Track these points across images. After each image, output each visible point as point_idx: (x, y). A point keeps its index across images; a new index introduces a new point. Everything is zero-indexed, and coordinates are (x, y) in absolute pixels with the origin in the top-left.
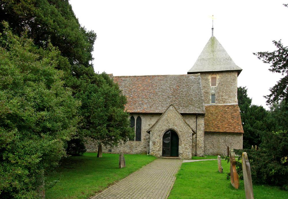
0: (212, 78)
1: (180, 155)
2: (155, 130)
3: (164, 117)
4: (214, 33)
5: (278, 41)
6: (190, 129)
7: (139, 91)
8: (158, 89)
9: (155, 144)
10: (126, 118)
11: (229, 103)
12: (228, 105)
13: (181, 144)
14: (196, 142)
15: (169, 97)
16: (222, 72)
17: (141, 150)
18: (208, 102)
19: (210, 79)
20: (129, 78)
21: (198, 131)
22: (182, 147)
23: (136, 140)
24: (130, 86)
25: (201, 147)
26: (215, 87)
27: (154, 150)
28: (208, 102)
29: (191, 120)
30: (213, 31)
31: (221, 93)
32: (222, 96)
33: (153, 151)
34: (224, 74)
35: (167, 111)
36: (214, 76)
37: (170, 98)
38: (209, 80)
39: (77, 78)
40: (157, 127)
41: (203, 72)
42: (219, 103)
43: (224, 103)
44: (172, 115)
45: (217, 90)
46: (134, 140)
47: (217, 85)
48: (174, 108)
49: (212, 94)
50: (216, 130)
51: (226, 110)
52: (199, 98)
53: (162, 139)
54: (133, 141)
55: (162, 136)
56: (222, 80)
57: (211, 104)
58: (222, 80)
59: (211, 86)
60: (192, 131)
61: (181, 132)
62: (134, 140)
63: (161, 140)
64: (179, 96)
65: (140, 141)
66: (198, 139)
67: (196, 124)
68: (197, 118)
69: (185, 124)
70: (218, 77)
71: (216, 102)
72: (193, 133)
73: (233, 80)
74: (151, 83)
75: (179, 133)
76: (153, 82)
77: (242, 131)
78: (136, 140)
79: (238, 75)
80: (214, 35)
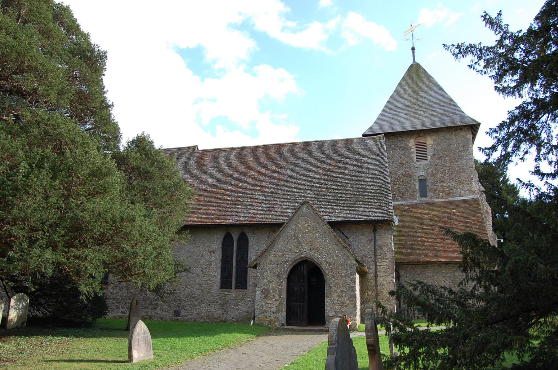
0: (417, 145)
2: (268, 261)
3: (289, 232)
4: (415, 53)
5: (493, 15)
6: (351, 258)
7: (247, 178)
8: (289, 170)
9: (267, 295)
11: (460, 196)
14: (377, 286)
15: (311, 187)
16: (437, 132)
17: (247, 311)
18: (413, 197)
19: (412, 147)
21: (380, 260)
22: (331, 300)
23: (236, 288)
24: (229, 169)
26: (425, 162)
28: (413, 197)
30: (413, 53)
31: (439, 175)
32: (443, 182)
33: (263, 313)
34: (442, 135)
35: (295, 217)
36: (421, 140)
37: (315, 189)
38: (411, 148)
40: (271, 257)
41: (397, 132)
42: (438, 196)
43: (448, 197)
44: (306, 225)
45: (430, 170)
46: (231, 288)
47: (429, 158)
48: (310, 208)
49: (420, 178)
50: (431, 258)
51: (454, 211)
52: (381, 187)
53: (284, 283)
54: (229, 290)
55: (285, 276)
56: (439, 148)
57: (419, 199)
58: (439, 148)
59: (415, 160)
60: (355, 263)
61: (329, 264)
62: (231, 288)
64: (334, 183)
65: (246, 288)
66: (381, 279)
67: (375, 245)
68: (375, 231)
69: (337, 245)
70: (430, 141)
71: (430, 194)
72: (357, 265)
73: (463, 146)
74: (276, 159)
75: (325, 268)
76: (279, 158)
78: (236, 288)
80: (417, 60)
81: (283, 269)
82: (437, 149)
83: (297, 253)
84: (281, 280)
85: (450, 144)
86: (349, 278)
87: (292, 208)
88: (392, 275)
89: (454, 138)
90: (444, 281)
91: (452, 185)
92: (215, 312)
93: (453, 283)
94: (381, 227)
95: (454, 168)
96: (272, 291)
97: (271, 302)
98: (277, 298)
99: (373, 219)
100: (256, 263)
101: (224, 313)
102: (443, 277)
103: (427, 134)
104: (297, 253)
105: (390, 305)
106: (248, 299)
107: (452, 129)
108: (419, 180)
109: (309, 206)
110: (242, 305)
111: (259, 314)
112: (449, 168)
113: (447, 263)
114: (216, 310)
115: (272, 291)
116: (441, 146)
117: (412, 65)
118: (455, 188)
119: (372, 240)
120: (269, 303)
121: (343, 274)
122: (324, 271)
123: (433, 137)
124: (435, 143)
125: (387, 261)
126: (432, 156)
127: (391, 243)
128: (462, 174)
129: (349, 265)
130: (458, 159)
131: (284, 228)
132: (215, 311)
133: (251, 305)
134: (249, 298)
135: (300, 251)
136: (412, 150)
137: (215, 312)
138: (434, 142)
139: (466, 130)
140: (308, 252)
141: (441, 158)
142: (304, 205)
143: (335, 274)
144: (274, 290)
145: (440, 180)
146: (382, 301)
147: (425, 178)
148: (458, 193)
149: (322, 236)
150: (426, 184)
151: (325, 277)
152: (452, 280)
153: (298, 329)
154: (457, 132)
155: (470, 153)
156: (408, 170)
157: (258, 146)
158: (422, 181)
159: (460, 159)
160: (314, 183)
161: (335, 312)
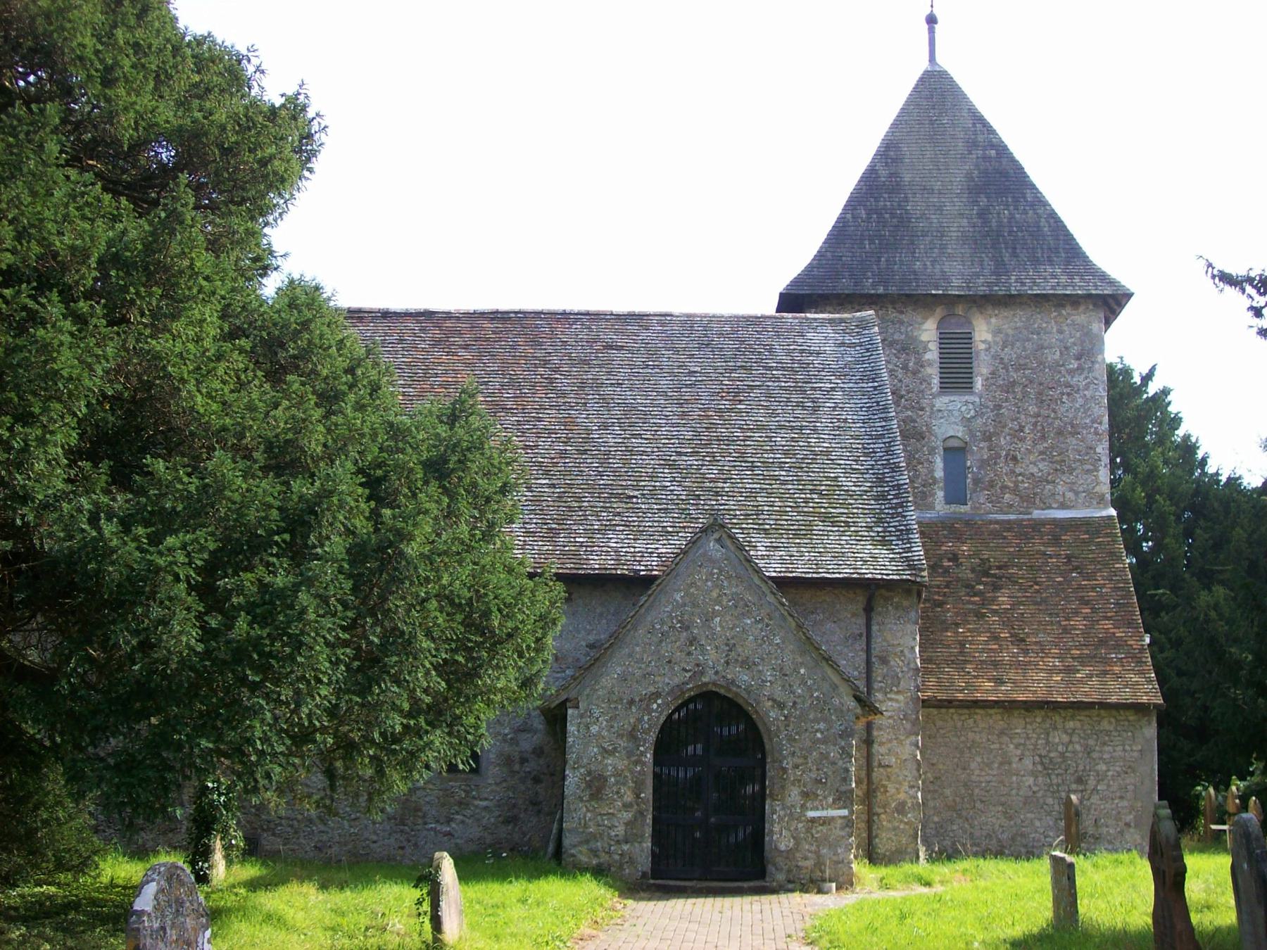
1: (774, 865)
6: (844, 689)
9: (599, 790)
10: (149, 530)
11: (1063, 506)
12: (1056, 522)
13: (783, 787)
20: (382, 326)
25: (901, 808)
27: (594, 837)
29: (829, 625)
30: (931, 32)
33: (587, 842)
39: (428, 460)
47: (979, 384)
48: (728, 542)
55: (652, 737)
56: (1008, 354)
61: (781, 706)
63: (644, 764)
69: (803, 653)
73: (1078, 358)
77: (1148, 692)
79: (1108, 323)
81: (646, 718)
82: (1002, 359)
83: (690, 671)
84: (642, 749)
85: (1042, 347)
86: (835, 745)
87: (621, 528)
88: (913, 738)
89: (1055, 330)
90: (1017, 759)
91: (1041, 471)
92: (375, 842)
93: (1042, 763)
94: (886, 599)
95: (1050, 421)
96: (613, 779)
97: (611, 811)
98: (629, 799)
99: (869, 576)
100: (565, 697)
101: (405, 843)
102: (1017, 747)
103: (975, 309)
104: (690, 671)
105: (906, 823)
106: (484, 803)
107: (1049, 300)
108: (945, 449)
109: (724, 536)
110: (463, 822)
111: (575, 846)
112: (1034, 420)
113: (1029, 707)
114: (378, 835)
115: (613, 779)
116: (1015, 349)
117: (926, 72)
118: (1048, 482)
119: (861, 635)
120: (604, 815)
121: (819, 735)
122: (765, 724)
123: (993, 320)
124: (998, 339)
125: (901, 698)
126: (987, 379)
127: (913, 648)
128: (1072, 441)
129: (835, 710)
130: (1063, 394)
131: (651, 599)
132: (375, 838)
133: (492, 820)
134: (486, 799)
135: (698, 665)
136: (928, 356)
137: (375, 842)
138: (994, 336)
139: (1091, 307)
140: (720, 668)
141: (1013, 386)
142: (709, 532)
143: (797, 733)
144: (620, 775)
145: (1007, 455)
146: (882, 811)
147: (963, 445)
148: (1057, 497)
149: (760, 626)
150: (965, 462)
151: (766, 741)
152: (1040, 756)
153: (691, 887)
154: (1064, 312)
155: (1096, 379)
156: (915, 417)
157: (475, 313)
158: (955, 453)
159: (1068, 394)
160: (679, 454)
161: (794, 838)
